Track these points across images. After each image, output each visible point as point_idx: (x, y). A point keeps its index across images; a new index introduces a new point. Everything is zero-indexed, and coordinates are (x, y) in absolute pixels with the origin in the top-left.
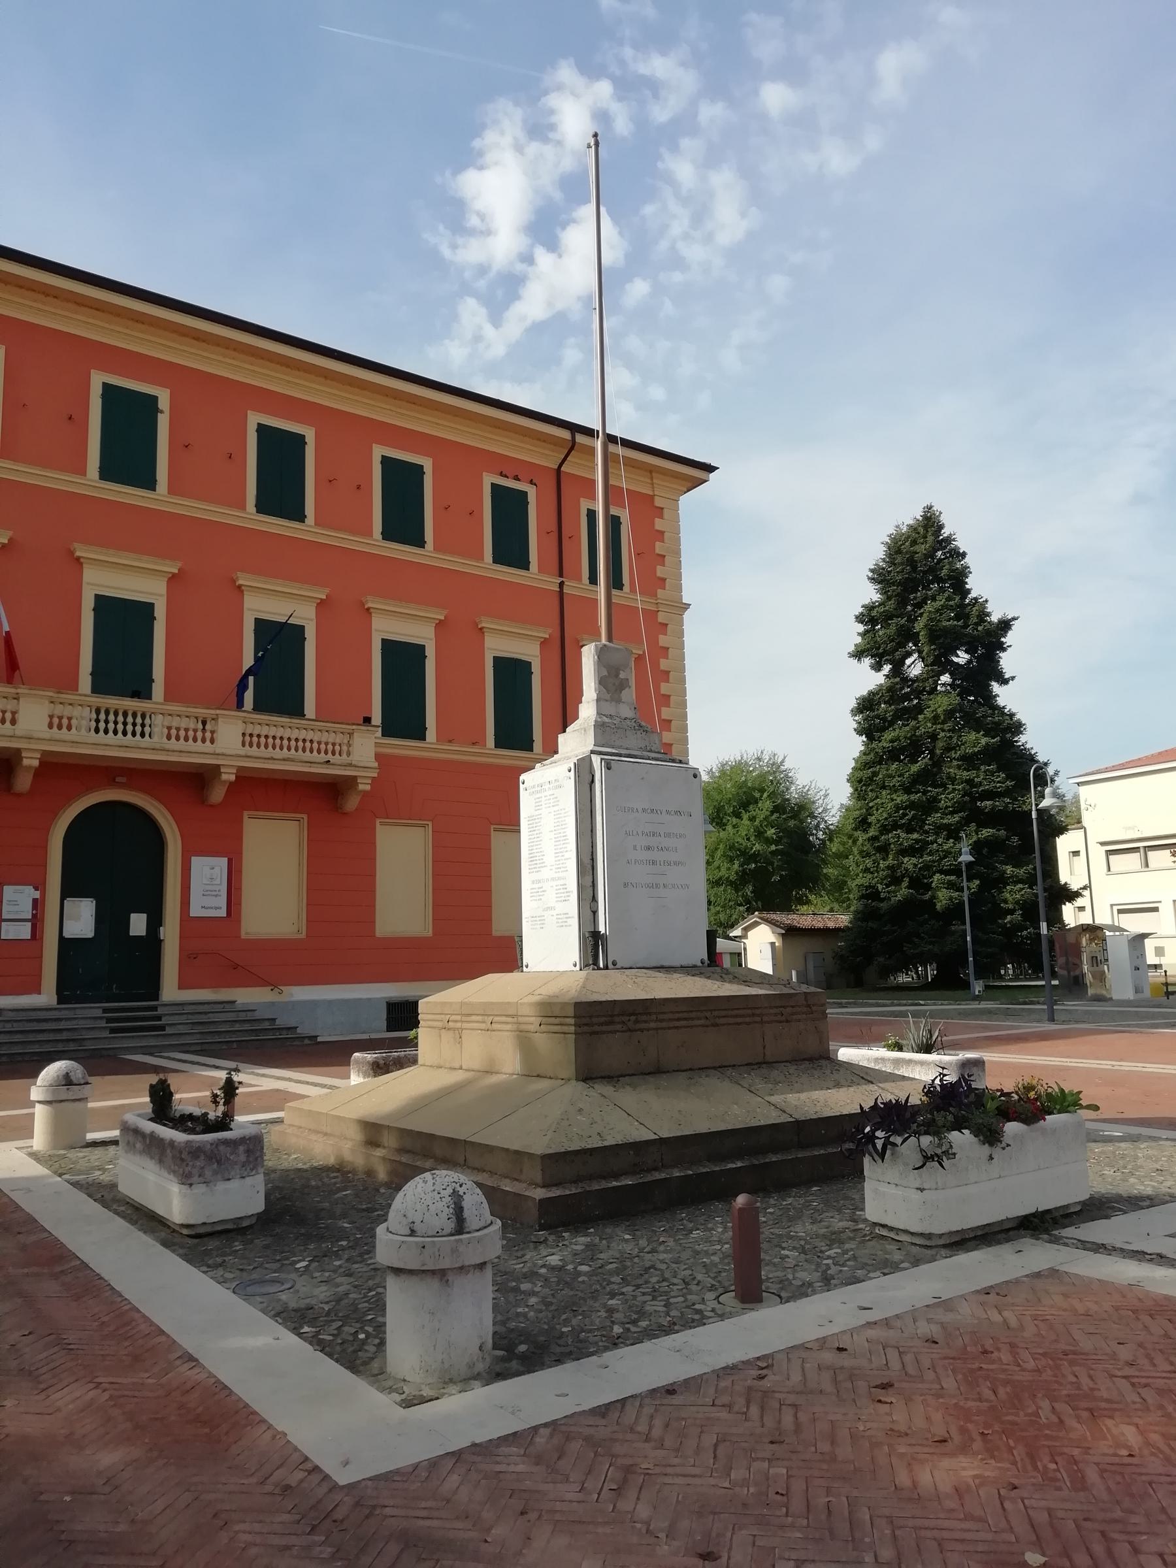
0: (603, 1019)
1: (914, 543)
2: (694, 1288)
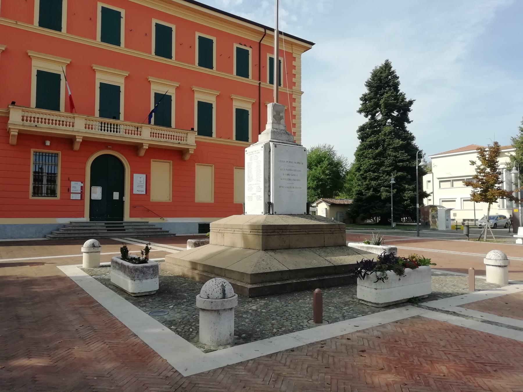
0: (271, 231)
1: (381, 73)
2: (300, 318)
